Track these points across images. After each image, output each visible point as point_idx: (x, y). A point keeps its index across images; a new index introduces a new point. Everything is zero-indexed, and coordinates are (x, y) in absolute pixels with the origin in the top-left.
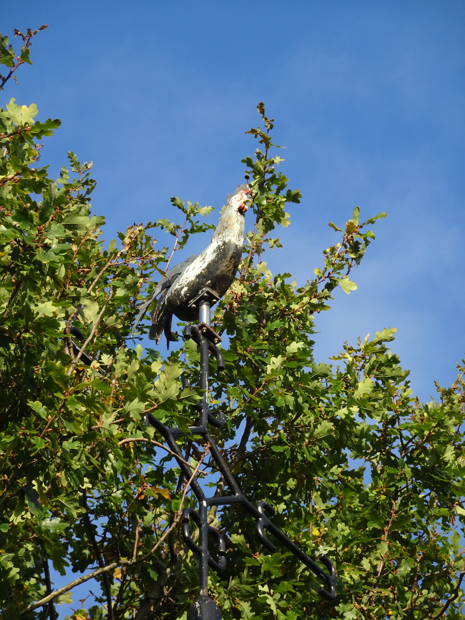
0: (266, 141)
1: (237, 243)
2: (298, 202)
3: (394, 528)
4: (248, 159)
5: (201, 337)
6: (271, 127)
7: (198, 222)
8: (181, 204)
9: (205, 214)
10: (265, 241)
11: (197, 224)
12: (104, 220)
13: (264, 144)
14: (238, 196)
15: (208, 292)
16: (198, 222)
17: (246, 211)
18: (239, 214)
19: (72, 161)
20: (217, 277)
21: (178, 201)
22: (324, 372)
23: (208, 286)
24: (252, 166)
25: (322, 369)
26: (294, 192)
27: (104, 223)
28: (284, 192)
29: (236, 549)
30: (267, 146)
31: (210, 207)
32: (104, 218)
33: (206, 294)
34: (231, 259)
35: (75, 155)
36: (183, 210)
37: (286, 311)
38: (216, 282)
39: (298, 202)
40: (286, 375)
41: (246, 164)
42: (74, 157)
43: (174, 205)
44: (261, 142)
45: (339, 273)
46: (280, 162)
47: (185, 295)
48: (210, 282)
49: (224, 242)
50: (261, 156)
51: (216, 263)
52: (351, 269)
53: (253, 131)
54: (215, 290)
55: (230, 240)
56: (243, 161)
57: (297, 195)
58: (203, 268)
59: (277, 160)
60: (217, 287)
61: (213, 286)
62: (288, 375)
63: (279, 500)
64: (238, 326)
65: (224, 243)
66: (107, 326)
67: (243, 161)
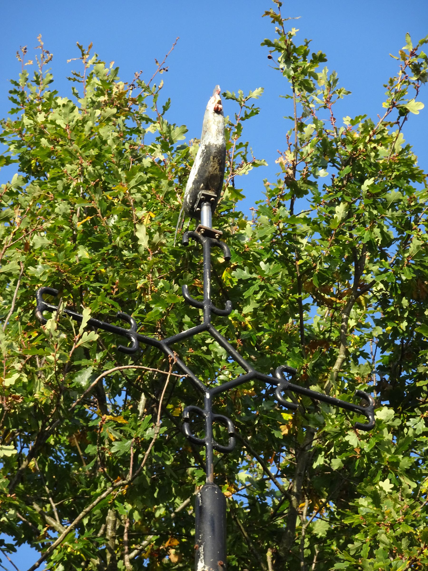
0: (277, 19)
1: (216, 143)
2: (325, 60)
3: (324, 386)
4: (266, 41)
5: (202, 238)
6: (280, 5)
7: (253, 105)
8: (233, 96)
9: (257, 96)
10: (333, 94)
11: (253, 107)
12: (186, 128)
13: (277, 23)
14: (212, 99)
15: (203, 195)
16: (253, 105)
17: (221, 110)
18: (216, 114)
19: (143, 88)
20: (207, 178)
21: (229, 94)
22: (397, 198)
23: (202, 189)
24: (273, 45)
25: (394, 196)
26: (318, 54)
27: (187, 131)
28: (309, 57)
29: (164, 468)
30: (281, 23)
31: (260, 89)
32: (185, 126)
33: (202, 197)
34: (214, 159)
35: (143, 82)
36: (236, 100)
37: (354, 155)
38: (207, 183)
39: (325, 60)
40: (369, 211)
41: (266, 46)
42: (143, 84)
43: (227, 99)
44: (273, 22)
45: (403, 99)
46: (296, 32)
47: (190, 202)
48: (202, 185)
49: (206, 145)
50: (281, 32)
51: (203, 166)
52: (419, 89)
53: (267, 13)
54: (210, 190)
55: (209, 143)
56: (263, 44)
57: (321, 55)
58: (196, 174)
59: (293, 31)
60: (210, 187)
61: (207, 188)
62: (371, 210)
63: (401, 319)
64: (302, 188)
65: (206, 147)
66: (155, 243)
67: (263, 44)
